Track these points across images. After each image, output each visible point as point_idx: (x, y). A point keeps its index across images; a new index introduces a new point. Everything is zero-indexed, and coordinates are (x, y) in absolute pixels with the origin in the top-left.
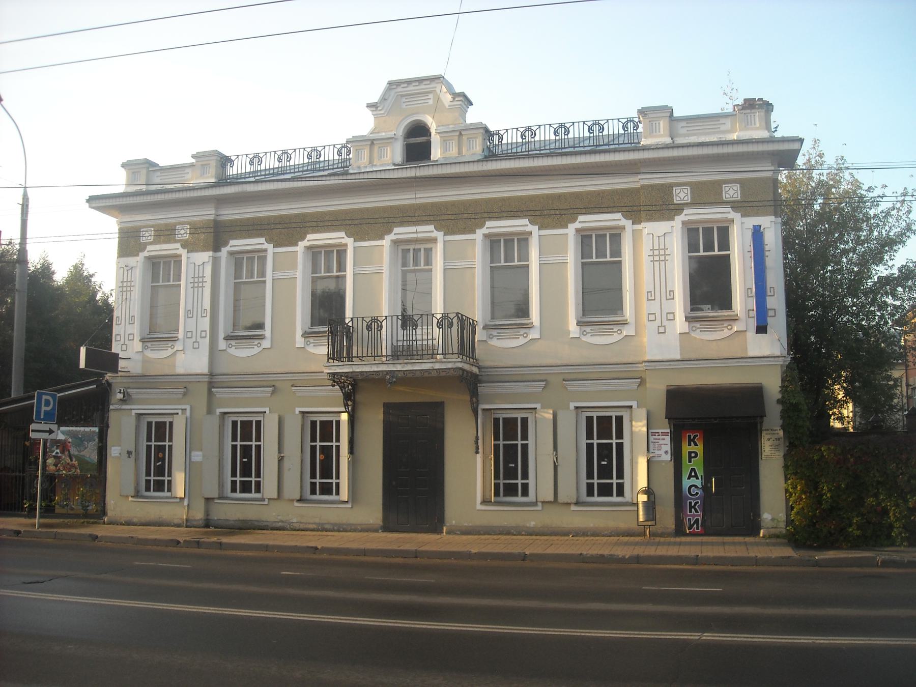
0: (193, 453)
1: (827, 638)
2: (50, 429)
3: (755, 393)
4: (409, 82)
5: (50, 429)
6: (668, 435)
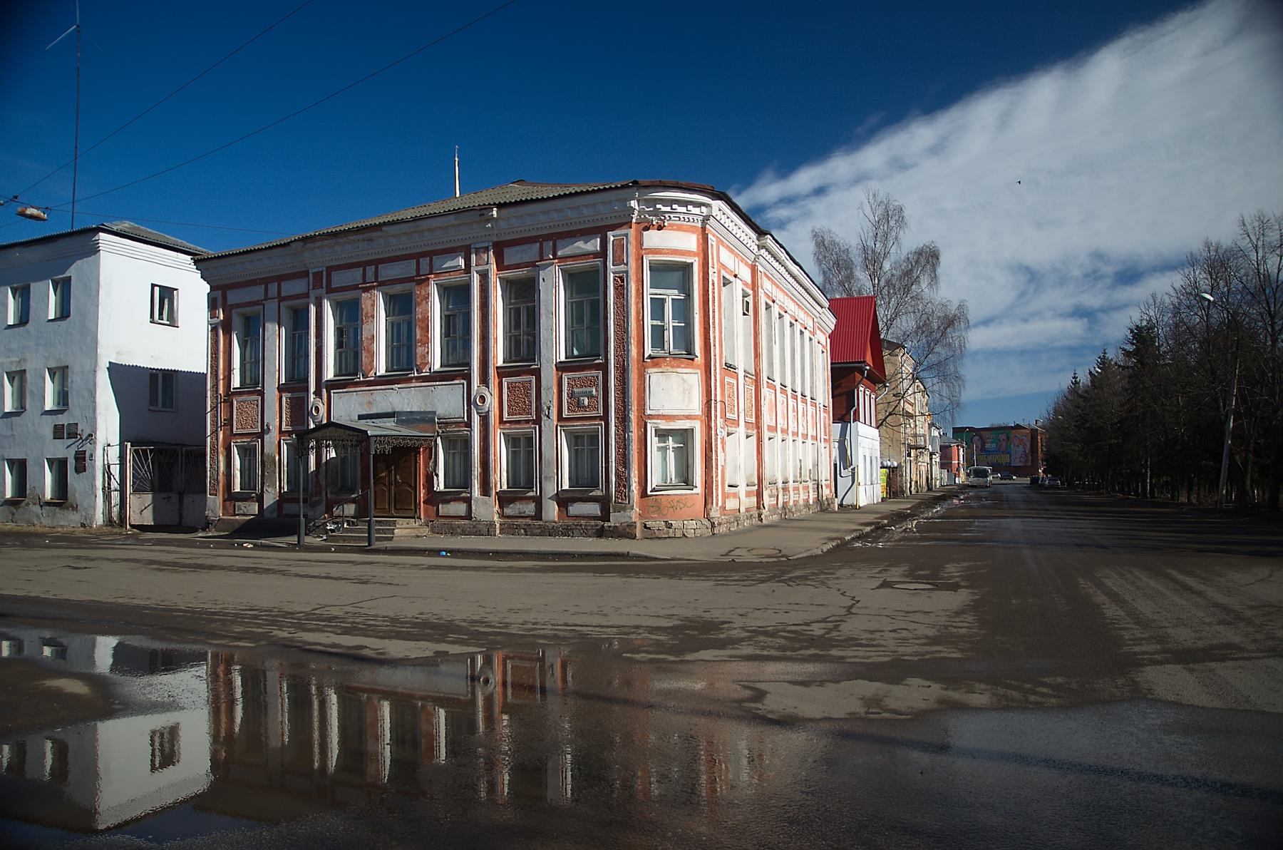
0: (696, 407)
1: (344, 390)
2: (110, 363)
3: (57, 651)
4: (566, 341)
5: (110, 363)
6: (234, 389)
